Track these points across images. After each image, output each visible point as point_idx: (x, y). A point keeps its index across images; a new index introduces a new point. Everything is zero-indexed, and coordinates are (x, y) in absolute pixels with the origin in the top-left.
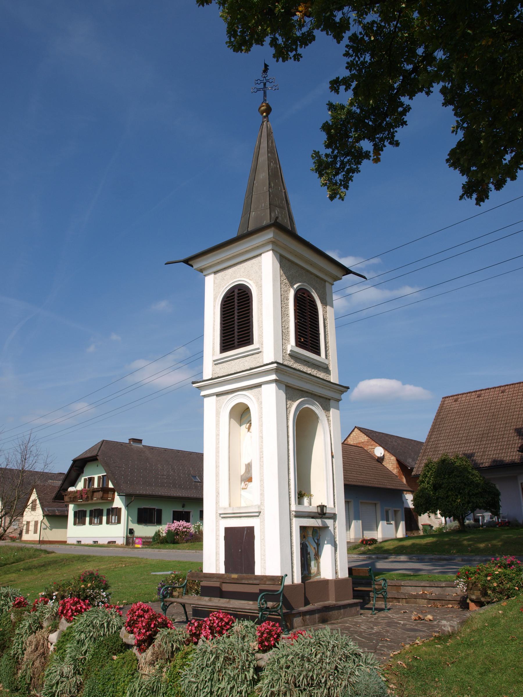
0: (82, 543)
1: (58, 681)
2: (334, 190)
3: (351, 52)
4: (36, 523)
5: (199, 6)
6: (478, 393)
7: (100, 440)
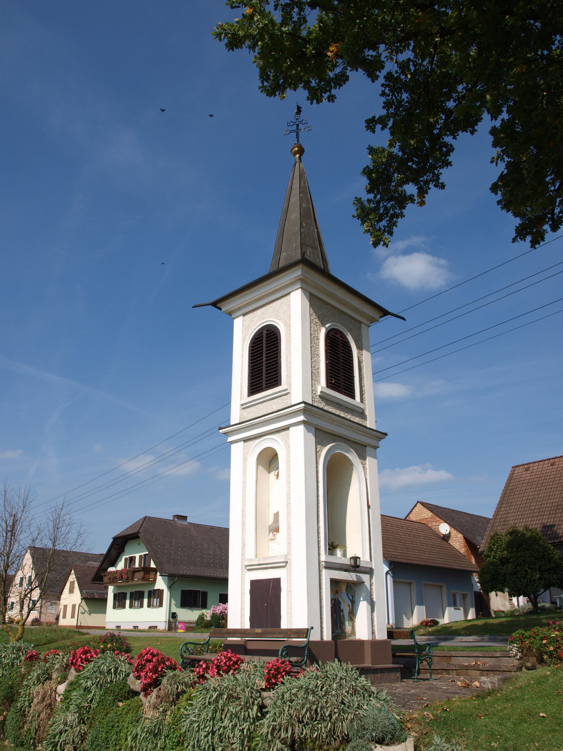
0: (122, 628)
1: (61, 731)
2: (377, 236)
3: (387, 91)
4: (74, 606)
5: (229, 50)
6: (551, 461)
7: (142, 516)
